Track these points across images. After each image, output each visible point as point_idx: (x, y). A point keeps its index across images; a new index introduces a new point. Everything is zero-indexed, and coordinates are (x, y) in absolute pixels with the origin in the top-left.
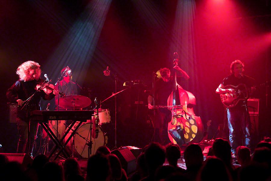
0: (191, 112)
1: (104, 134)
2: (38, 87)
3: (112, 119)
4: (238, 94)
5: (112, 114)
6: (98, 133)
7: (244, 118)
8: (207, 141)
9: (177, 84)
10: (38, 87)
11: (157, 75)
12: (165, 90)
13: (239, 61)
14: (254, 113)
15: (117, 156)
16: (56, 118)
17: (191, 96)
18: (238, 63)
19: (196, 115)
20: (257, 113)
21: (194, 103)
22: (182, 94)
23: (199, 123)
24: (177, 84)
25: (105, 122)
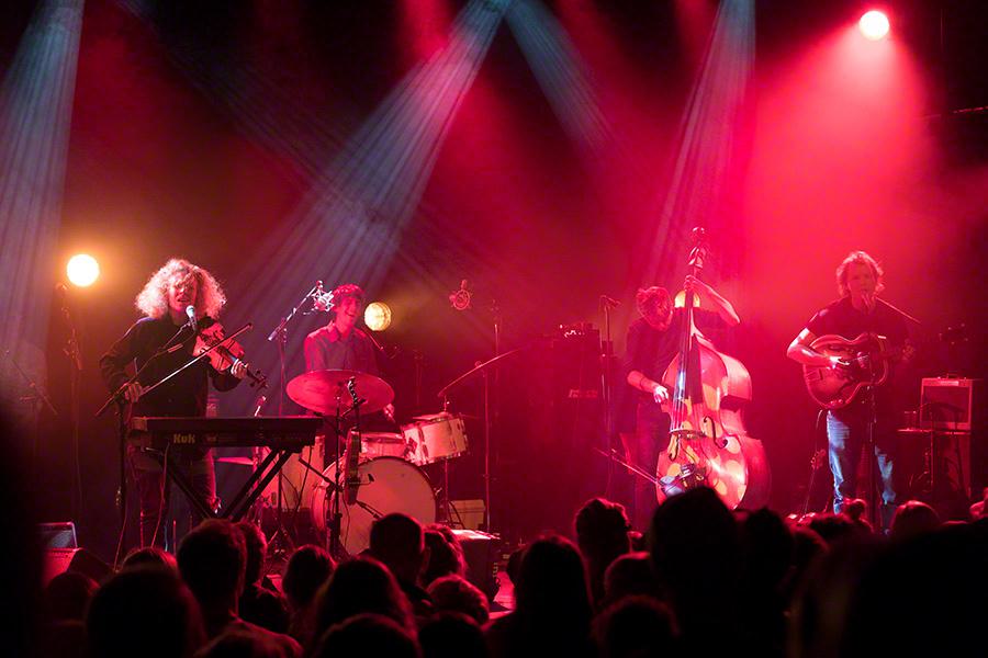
0: (731, 423)
1: (434, 492)
2: (905, 358)
3: (471, 443)
4: (854, 365)
5: (471, 431)
6: (357, 486)
7: (119, 434)
8: (798, 519)
9: (694, 330)
10: (905, 358)
11: (325, 290)
12: (658, 345)
13: (867, 257)
14: (956, 425)
15: (391, 570)
16: (195, 439)
17: (737, 372)
18: (859, 262)
19: (750, 435)
20: (966, 426)
21: (745, 394)
22: (706, 362)
23: (756, 460)
24: (694, 330)
25: (447, 454)
